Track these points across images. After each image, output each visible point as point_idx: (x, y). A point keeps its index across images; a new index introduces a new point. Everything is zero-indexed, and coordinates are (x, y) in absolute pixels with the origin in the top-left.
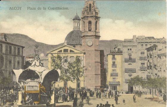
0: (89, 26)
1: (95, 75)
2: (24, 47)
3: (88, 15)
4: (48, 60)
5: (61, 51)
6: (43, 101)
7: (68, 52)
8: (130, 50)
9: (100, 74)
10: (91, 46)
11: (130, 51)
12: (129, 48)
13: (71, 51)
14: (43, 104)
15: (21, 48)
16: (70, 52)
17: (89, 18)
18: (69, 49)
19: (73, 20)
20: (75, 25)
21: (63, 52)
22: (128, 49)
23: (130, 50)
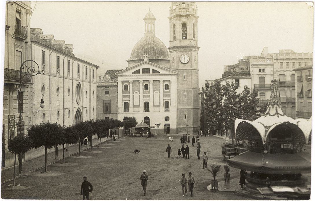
0: (182, 31)
1: (192, 110)
2: (99, 67)
3: (181, 13)
4: (98, 87)
5: (138, 71)
6: (185, 151)
7: (149, 73)
8: (262, 70)
9: (17, 108)
10: (187, 63)
11: (262, 73)
12: (262, 67)
13: (154, 71)
14: (246, 152)
15: (95, 69)
16: (153, 73)
17: (182, 18)
18: (151, 68)
19: (144, 19)
20: (151, 27)
21: (141, 72)
22: (260, 70)
23: (262, 70)
